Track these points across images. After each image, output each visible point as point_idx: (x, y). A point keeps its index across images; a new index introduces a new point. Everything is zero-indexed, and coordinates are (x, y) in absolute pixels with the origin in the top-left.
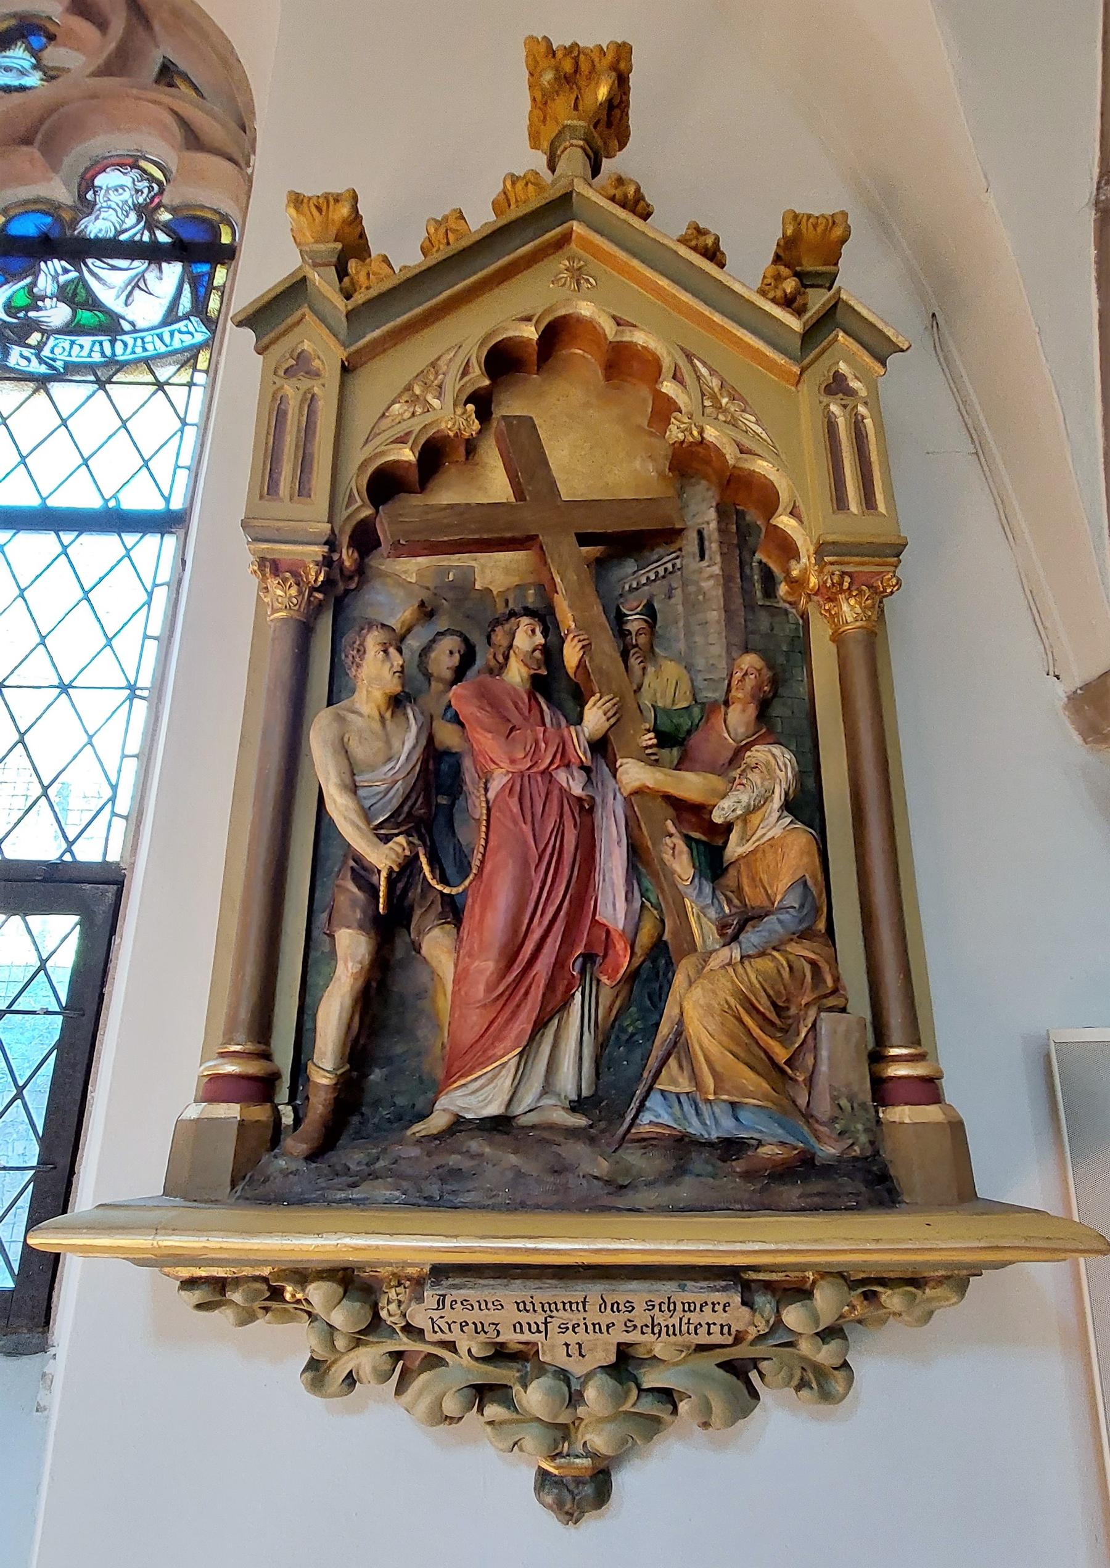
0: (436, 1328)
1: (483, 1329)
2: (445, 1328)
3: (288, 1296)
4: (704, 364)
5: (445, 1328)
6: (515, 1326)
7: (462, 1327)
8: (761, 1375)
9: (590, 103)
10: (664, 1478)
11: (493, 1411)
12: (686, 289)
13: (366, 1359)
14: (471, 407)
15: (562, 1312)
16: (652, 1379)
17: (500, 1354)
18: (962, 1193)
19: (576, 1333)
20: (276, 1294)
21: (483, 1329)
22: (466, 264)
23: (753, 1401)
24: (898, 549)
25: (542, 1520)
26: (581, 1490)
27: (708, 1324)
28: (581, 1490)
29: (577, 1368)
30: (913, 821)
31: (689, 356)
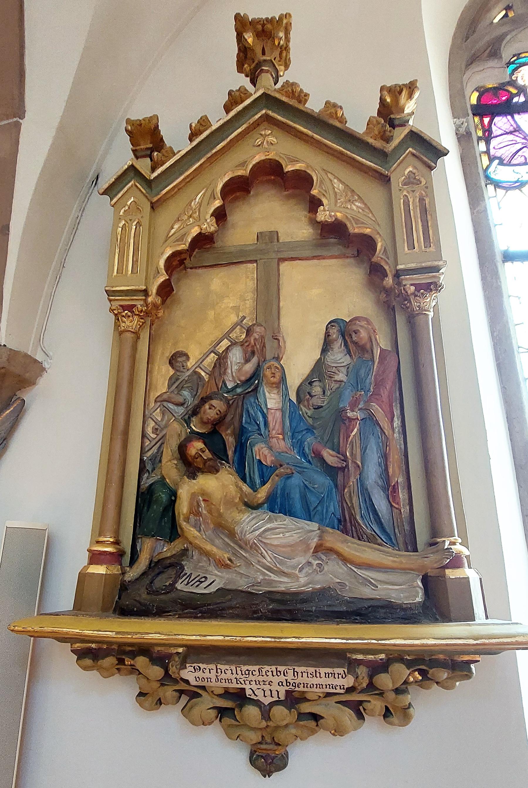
0: (238, 682)
1: (259, 683)
2: (243, 682)
3: (126, 663)
4: (170, 232)
5: (243, 682)
6: (279, 683)
7: (250, 682)
8: (364, 709)
9: (260, 43)
11: (227, 721)
12: (187, 153)
13: (169, 692)
15: (315, 678)
16: (306, 708)
17: (227, 694)
19: (266, 683)
20: (121, 661)
21: (259, 683)
22: (207, 141)
23: (361, 721)
24: (437, 269)
25: (253, 776)
26: (268, 760)
27: (302, 672)
28: (268, 760)
30: (490, 347)
31: (167, 238)
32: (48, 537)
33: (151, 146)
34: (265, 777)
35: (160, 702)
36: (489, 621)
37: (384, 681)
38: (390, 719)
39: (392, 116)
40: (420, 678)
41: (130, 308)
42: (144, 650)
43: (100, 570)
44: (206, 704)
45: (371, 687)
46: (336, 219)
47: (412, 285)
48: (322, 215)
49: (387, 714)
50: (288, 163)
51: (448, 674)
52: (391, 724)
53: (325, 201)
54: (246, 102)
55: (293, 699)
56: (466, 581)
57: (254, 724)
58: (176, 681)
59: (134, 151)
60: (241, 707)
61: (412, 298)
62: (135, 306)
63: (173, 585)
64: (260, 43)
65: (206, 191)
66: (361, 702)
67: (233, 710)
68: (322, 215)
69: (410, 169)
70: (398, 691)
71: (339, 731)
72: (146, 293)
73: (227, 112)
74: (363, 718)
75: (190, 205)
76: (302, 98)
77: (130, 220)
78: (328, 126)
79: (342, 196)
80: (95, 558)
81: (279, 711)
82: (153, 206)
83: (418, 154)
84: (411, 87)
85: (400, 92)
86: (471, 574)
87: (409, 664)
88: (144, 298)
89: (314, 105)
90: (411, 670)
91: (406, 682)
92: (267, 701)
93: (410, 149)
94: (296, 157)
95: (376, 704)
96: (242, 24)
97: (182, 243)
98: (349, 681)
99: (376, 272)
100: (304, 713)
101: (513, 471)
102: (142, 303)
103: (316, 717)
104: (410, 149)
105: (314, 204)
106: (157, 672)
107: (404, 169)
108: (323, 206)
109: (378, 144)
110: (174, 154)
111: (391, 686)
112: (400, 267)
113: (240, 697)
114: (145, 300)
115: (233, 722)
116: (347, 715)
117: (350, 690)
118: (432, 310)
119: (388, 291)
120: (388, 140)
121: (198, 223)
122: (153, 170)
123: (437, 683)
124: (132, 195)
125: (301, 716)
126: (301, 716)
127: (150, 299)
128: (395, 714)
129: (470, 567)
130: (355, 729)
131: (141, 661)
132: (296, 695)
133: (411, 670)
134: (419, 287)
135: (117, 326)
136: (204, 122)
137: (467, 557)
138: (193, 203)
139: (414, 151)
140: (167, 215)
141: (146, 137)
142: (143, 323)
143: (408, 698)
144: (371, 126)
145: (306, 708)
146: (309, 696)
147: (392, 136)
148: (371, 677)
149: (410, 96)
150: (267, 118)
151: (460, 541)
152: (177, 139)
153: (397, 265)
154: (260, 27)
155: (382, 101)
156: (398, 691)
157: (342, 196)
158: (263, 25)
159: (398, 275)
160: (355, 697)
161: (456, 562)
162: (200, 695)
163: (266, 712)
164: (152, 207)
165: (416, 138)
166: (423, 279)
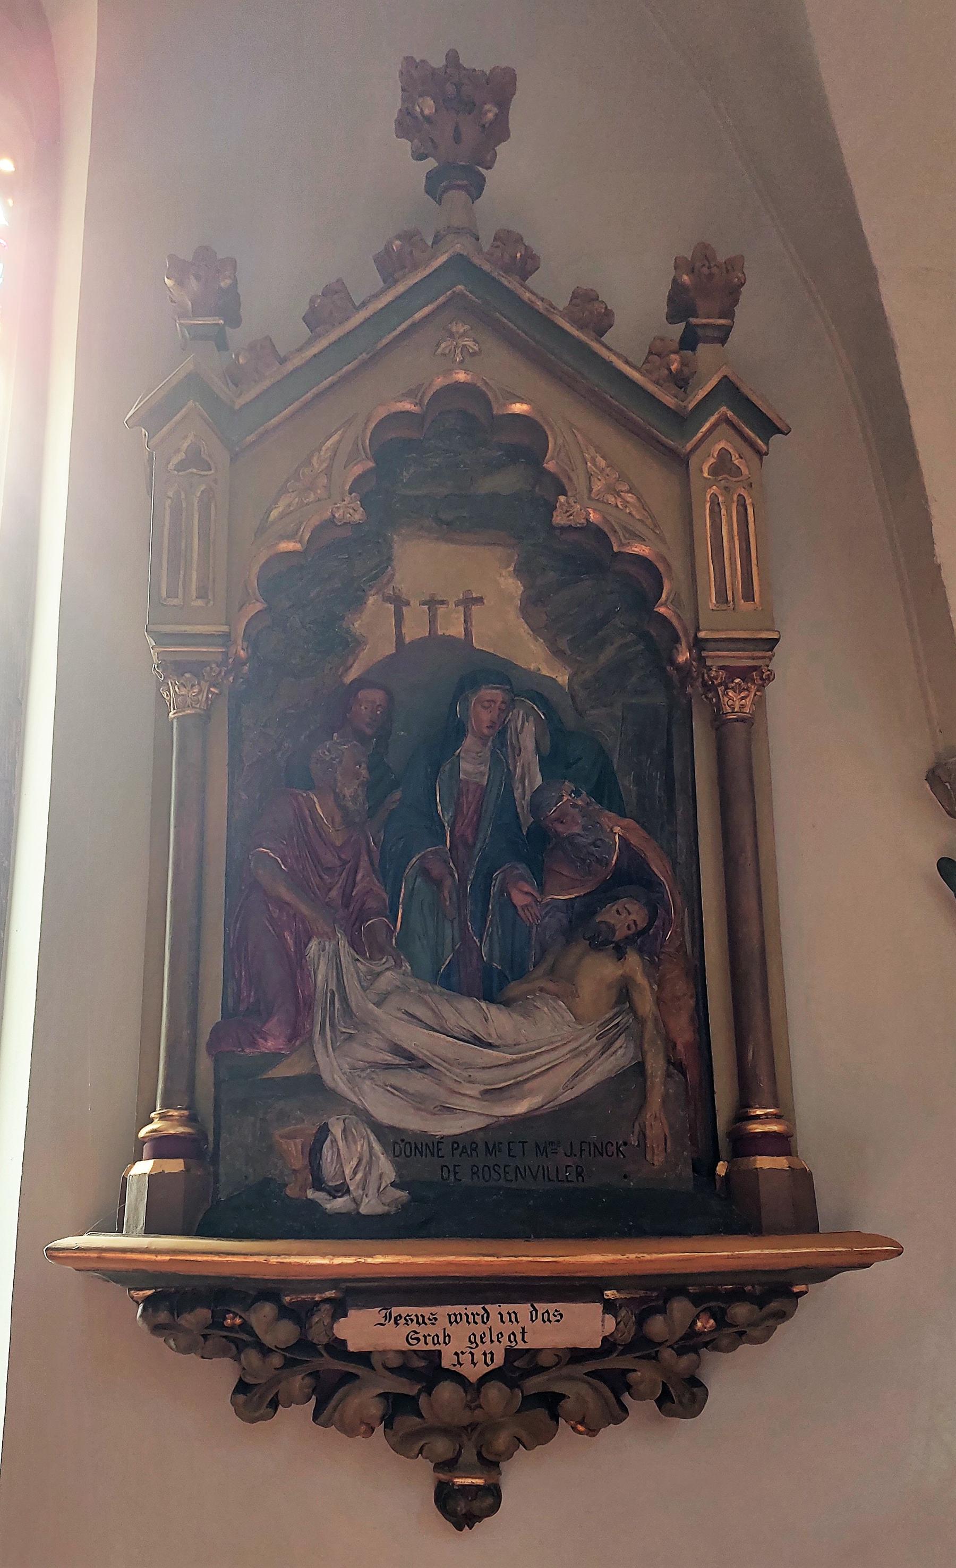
9: (459, 115)
10: (530, 1481)
11: (409, 1422)
16: (535, 1384)
18: (804, 1220)
26: (465, 1507)
28: (465, 1507)
29: (473, 1373)
34: (460, 1528)
35: (274, 1404)
38: (668, 1405)
42: (267, 1291)
44: (364, 1400)
45: (642, 1346)
47: (721, 668)
49: (664, 1400)
55: (519, 1365)
60: (429, 1390)
61: (720, 690)
62: (208, 664)
63: (678, 668)
65: (342, 437)
66: (625, 1372)
67: (414, 1400)
69: (722, 444)
75: (310, 463)
81: (495, 1393)
83: (736, 420)
87: (697, 1300)
90: (699, 1309)
92: (473, 1373)
93: (723, 409)
95: (643, 1374)
97: (670, 600)
104: (723, 409)
107: (715, 442)
112: (702, 635)
113: (428, 1369)
120: (681, 382)
126: (531, 1401)
133: (699, 1309)
134: (732, 672)
138: (315, 458)
139: (730, 413)
145: (535, 1384)
146: (544, 1360)
153: (698, 629)
154: (450, 89)
159: (698, 644)
160: (614, 1362)
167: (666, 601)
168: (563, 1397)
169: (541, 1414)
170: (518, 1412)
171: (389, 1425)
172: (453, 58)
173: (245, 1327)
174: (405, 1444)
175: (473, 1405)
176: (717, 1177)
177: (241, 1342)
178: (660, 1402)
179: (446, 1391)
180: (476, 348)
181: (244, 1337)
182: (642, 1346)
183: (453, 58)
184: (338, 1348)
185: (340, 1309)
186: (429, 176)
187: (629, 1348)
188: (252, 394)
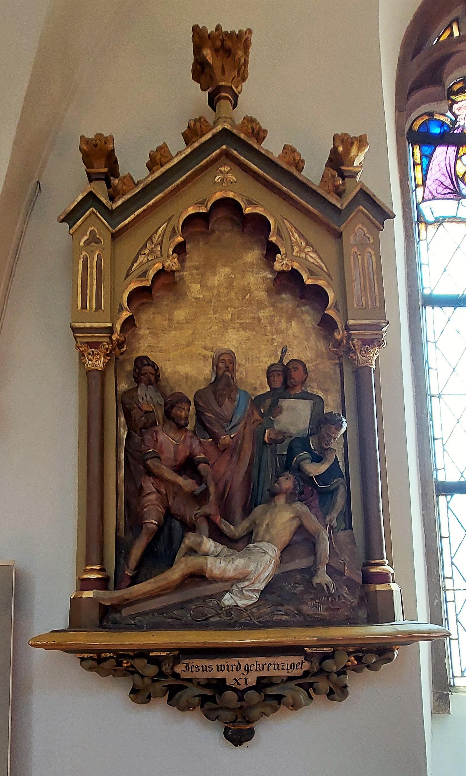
9: (219, 59)
10: (275, 732)
11: (209, 705)
14: (175, 255)
16: (271, 691)
20: (120, 664)
22: (169, 176)
26: (239, 735)
28: (239, 735)
32: (15, 573)
33: (106, 170)
35: (149, 697)
36: (406, 622)
37: (331, 665)
39: (342, 168)
40: (356, 662)
41: (92, 345)
42: (142, 653)
43: (88, 594)
45: (321, 671)
46: (292, 269)
48: (281, 264)
50: (247, 206)
51: (376, 658)
52: (334, 700)
53: (282, 250)
54: (206, 136)
55: (263, 684)
56: (391, 592)
57: (232, 705)
58: (165, 676)
59: (88, 174)
60: (221, 694)
64: (219, 59)
68: (281, 264)
70: (339, 673)
71: (295, 706)
72: (111, 330)
73: (188, 141)
74: (312, 699)
76: (259, 135)
77: (92, 251)
78: (281, 175)
79: (302, 250)
80: (84, 584)
82: (114, 236)
84: (362, 142)
85: (352, 144)
86: (394, 587)
88: (110, 335)
89: (272, 147)
91: (346, 666)
93: (91, 209)
94: (257, 203)
95: (323, 685)
96: (200, 37)
98: (306, 666)
99: (327, 325)
100: (271, 696)
101: (430, 681)
102: (108, 340)
103: (279, 698)
105: (272, 251)
106: (152, 670)
107: (356, 230)
108: (280, 254)
109: (332, 199)
110: (137, 185)
111: (335, 668)
112: (351, 322)
113: (219, 686)
114: (110, 337)
115: (214, 706)
116: (302, 695)
117: (306, 674)
118: (374, 364)
119: (338, 344)
121: (161, 259)
122: (112, 199)
123: (368, 667)
124: (94, 223)
125: (268, 697)
127: (114, 337)
128: (337, 693)
129: (394, 582)
130: (308, 705)
131: (140, 664)
132: (265, 681)
135: (82, 363)
136: (163, 149)
137: (392, 574)
140: (129, 246)
141: (100, 157)
142: (109, 360)
143: (348, 679)
144: (326, 179)
145: (271, 691)
146: (274, 681)
147: (345, 190)
148: (320, 663)
149: (360, 148)
150: (227, 154)
151: (387, 562)
152: (134, 166)
154: (219, 43)
155: (334, 151)
156: (339, 673)
157: (302, 250)
158: (223, 41)
161: (384, 578)
162: (186, 687)
163: (241, 694)
164: (112, 237)
165: (366, 197)
166: (368, 334)
167: (331, 306)
168: (284, 696)
169: (274, 703)
170: (263, 702)
171: (202, 707)
172: (218, 28)
173: (132, 666)
174: (211, 715)
175: (241, 699)
176: (131, 388)
177: (132, 672)
178: (328, 695)
179: (230, 695)
180: (235, 180)
181: (133, 670)
182: (321, 671)
183: (218, 28)
184: (176, 676)
185: (177, 660)
186: (209, 94)
187: (315, 675)
188: (120, 202)
